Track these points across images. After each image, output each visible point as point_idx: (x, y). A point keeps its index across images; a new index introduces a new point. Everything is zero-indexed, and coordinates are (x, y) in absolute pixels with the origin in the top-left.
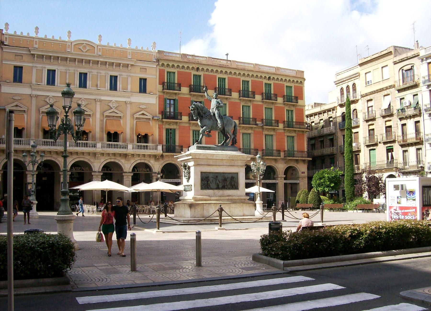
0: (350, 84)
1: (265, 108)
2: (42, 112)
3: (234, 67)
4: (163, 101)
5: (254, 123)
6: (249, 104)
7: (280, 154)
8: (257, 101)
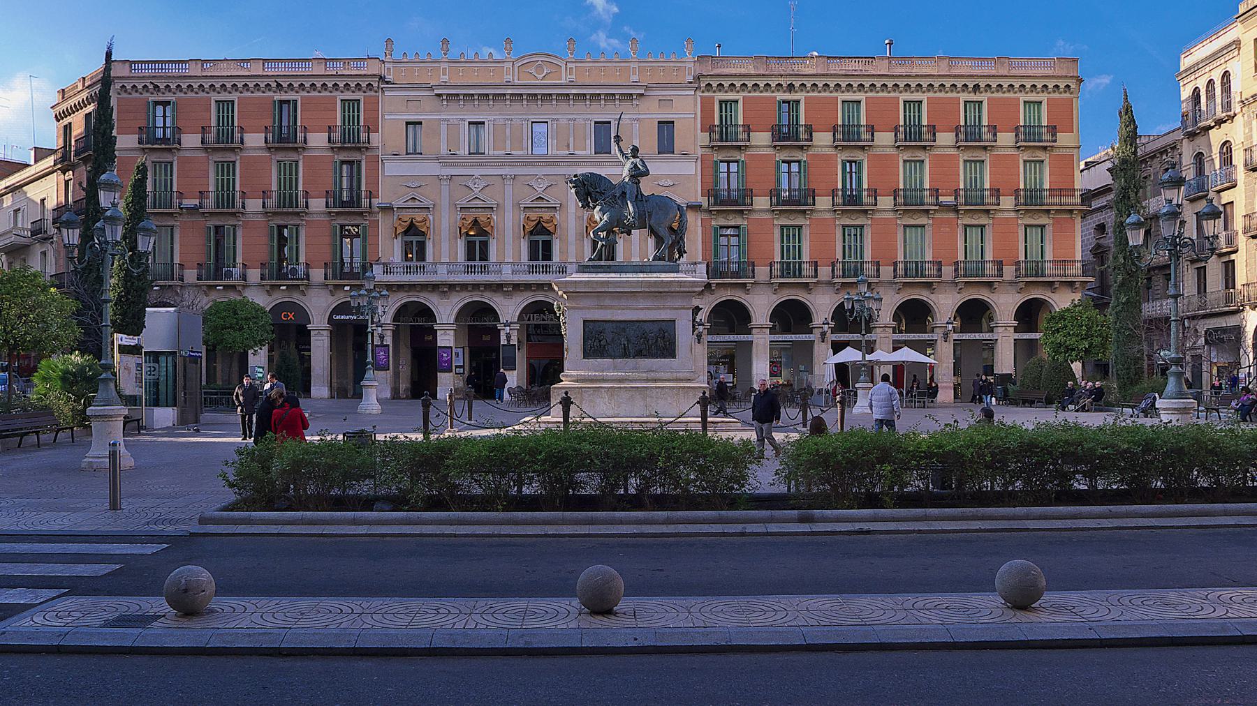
0: (1217, 76)
1: (905, 161)
4: (709, 169)
5: (933, 200)
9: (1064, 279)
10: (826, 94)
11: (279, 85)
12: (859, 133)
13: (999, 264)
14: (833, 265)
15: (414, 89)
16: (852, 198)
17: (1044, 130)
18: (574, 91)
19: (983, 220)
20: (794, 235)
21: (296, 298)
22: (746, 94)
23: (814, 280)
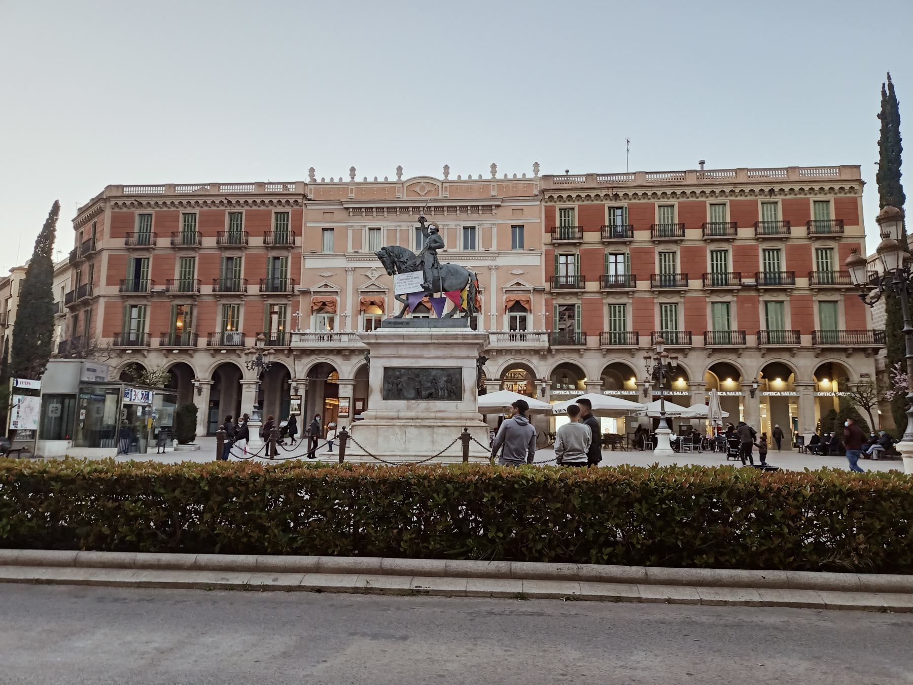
5: (736, 281)
9: (857, 346)
11: (229, 202)
14: (705, 334)
15: (330, 204)
17: (781, 224)
19: (782, 297)
22: (580, 203)
23: (636, 347)
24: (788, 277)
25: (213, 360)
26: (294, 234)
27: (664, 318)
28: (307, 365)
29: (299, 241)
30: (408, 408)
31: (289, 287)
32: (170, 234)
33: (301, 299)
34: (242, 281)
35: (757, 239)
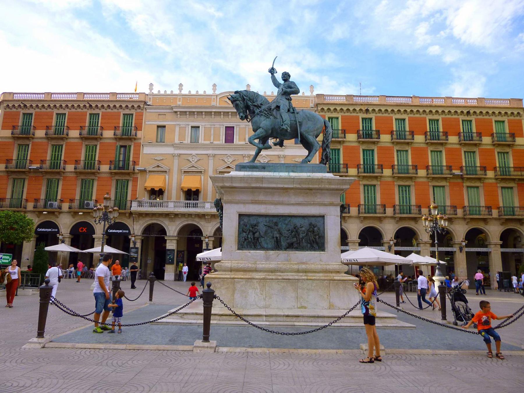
1: (465, 152)
2: (184, 172)
3: (416, 104)
5: (448, 172)
6: (372, 147)
7: (491, 211)
8: (349, 142)
10: (387, 115)
12: (405, 135)
13: (384, 206)
14: (359, 206)
15: (163, 109)
16: (369, 168)
18: (214, 110)
20: (406, 191)
21: (52, 219)
24: (378, 168)
25: (74, 220)
26: (136, 129)
27: (401, 196)
28: (144, 223)
29: (140, 134)
30: (267, 259)
31: (131, 167)
32: (11, 127)
33: (139, 176)
34: (96, 162)
35: (494, 145)
